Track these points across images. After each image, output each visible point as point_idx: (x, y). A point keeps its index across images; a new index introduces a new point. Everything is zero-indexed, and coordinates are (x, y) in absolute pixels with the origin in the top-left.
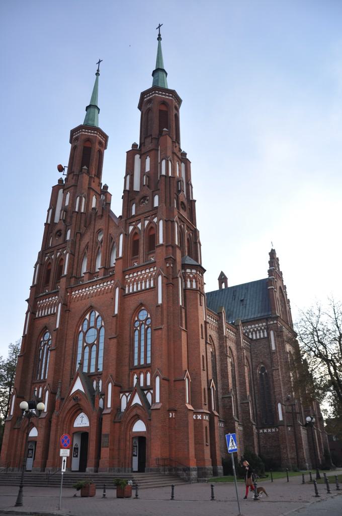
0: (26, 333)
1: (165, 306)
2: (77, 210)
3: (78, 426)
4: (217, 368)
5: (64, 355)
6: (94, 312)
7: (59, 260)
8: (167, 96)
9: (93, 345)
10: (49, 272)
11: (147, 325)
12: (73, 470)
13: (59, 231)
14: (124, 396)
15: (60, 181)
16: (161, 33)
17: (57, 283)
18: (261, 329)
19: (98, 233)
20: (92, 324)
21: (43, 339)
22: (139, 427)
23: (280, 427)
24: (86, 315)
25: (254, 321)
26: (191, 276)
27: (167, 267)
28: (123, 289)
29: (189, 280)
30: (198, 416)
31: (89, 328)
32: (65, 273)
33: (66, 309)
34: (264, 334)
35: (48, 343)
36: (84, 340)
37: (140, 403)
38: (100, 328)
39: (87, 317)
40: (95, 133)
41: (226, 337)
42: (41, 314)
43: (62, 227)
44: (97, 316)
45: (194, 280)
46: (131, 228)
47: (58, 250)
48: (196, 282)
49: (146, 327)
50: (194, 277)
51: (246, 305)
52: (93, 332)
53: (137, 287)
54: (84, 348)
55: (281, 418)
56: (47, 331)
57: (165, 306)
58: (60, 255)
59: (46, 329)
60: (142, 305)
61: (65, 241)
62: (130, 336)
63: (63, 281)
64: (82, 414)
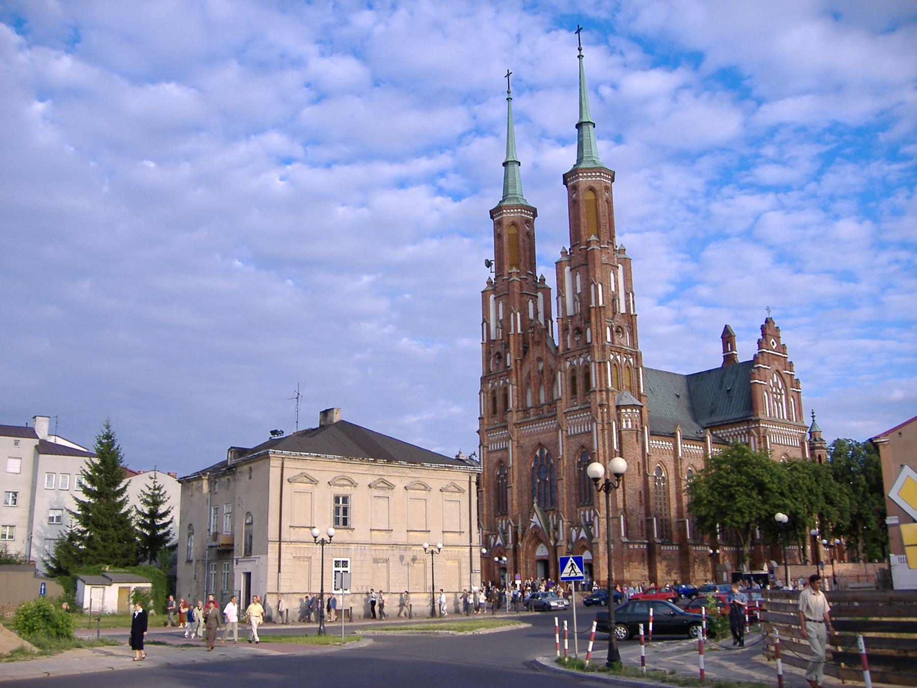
15: (489, 283)
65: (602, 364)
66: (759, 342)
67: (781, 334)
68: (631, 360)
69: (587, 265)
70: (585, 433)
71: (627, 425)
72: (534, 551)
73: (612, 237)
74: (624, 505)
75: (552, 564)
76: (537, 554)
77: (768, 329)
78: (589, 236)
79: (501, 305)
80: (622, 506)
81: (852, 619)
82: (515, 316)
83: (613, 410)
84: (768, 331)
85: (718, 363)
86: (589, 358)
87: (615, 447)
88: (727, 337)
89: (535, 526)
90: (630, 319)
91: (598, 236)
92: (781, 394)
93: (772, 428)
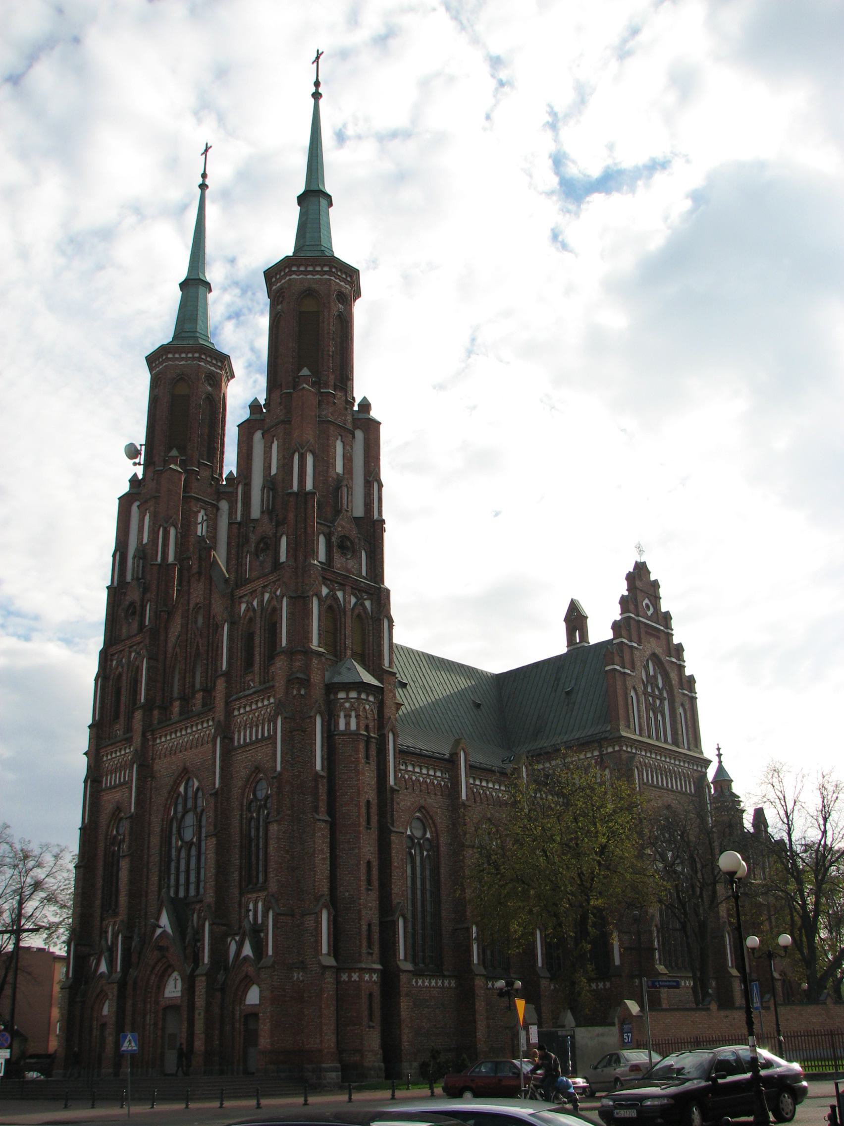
0: (86, 821)
2: (295, 488)
4: (442, 871)
5: (148, 863)
10: (118, 691)
13: (132, 604)
15: (134, 481)
16: (207, 172)
20: (190, 804)
21: (117, 831)
23: (613, 979)
24: (179, 785)
29: (342, 714)
32: (284, 644)
40: (326, 273)
42: (111, 783)
43: (267, 528)
45: (353, 714)
47: (130, 647)
48: (357, 716)
50: (352, 708)
52: (190, 819)
53: (251, 735)
54: (179, 851)
55: (617, 962)
58: (271, 599)
59: (120, 811)
61: (277, 565)
63: (138, 715)
65: (300, 603)
68: (368, 603)
71: (348, 724)
74: (333, 888)
77: (641, 586)
80: (325, 890)
81: (728, 947)
83: (318, 693)
87: (318, 767)
88: (575, 619)
89: (164, 932)
91: (315, 372)
92: (662, 700)
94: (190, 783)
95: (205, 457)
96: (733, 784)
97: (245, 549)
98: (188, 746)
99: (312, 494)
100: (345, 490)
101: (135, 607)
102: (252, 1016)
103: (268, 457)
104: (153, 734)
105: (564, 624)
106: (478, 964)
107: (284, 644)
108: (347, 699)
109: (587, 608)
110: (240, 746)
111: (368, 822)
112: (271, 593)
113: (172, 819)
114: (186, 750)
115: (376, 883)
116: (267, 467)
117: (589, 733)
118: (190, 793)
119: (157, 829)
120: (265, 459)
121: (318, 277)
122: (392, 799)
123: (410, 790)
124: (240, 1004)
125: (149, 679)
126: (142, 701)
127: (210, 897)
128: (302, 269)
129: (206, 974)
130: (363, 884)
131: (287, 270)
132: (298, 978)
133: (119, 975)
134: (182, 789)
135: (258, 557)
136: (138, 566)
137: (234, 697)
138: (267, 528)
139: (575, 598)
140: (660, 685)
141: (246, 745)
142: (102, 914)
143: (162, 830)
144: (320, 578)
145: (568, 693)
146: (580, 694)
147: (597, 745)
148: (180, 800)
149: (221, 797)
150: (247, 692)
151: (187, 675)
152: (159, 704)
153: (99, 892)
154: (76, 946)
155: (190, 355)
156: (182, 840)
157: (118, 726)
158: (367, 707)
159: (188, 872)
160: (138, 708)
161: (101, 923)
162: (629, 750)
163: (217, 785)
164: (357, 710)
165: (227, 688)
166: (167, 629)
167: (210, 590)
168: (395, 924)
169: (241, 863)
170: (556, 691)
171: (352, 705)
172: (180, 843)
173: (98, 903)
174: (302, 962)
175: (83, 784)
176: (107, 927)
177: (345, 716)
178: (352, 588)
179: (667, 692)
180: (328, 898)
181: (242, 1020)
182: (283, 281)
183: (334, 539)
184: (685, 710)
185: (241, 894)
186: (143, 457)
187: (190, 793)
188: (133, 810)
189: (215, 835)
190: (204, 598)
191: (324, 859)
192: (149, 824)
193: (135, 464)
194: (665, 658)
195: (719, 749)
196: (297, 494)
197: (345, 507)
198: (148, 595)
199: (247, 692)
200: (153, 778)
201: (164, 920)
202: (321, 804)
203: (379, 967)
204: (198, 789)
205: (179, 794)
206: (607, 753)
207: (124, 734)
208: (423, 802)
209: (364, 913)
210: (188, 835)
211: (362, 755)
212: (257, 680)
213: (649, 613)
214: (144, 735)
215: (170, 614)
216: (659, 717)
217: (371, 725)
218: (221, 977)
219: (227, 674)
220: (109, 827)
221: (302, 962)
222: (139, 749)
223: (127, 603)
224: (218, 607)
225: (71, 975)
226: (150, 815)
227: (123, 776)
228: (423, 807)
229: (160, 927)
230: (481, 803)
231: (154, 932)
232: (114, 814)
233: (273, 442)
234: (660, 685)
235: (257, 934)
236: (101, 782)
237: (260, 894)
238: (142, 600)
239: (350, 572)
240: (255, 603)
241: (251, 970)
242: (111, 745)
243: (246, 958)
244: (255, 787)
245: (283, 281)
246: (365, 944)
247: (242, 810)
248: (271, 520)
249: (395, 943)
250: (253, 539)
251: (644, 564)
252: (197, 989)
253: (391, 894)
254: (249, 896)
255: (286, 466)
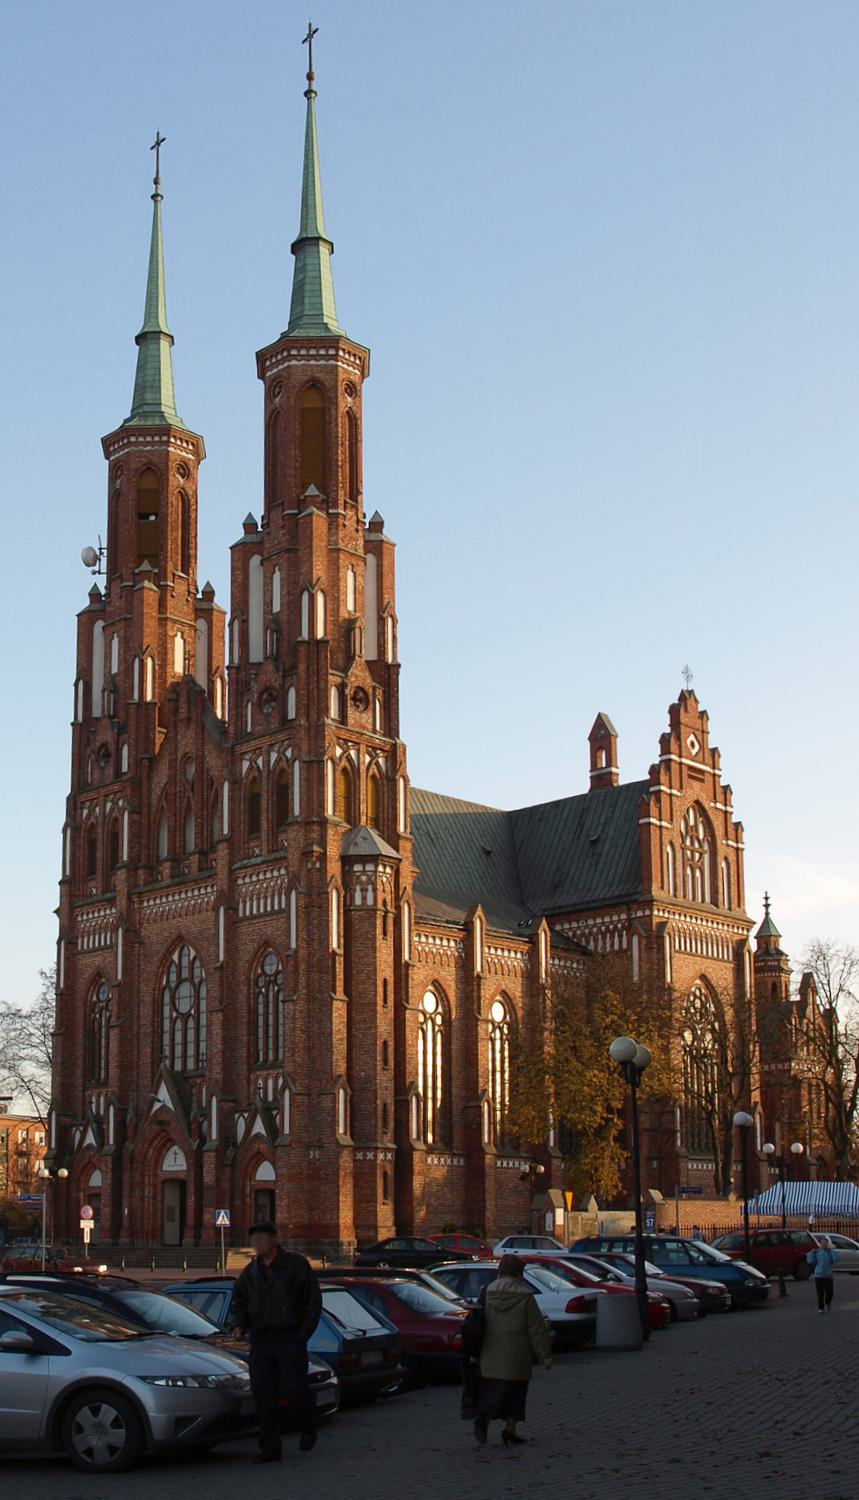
1: (302, 953)
2: (305, 635)
3: (171, 1169)
4: (453, 1047)
5: (138, 1033)
6: (186, 948)
7: (111, 820)
8: (322, 357)
9: (188, 1017)
10: (92, 844)
11: (278, 985)
12: (166, 1242)
13: (104, 745)
14: (241, 1118)
15: (94, 595)
17: (111, 875)
18: (616, 927)
19: (185, 763)
20: (185, 974)
21: (98, 997)
22: (266, 1172)
24: (172, 953)
25: (602, 907)
26: (364, 878)
27: (309, 870)
28: (232, 909)
29: (358, 888)
30: (368, 1153)
31: (180, 981)
32: (297, 812)
33: (133, 937)
34: (620, 942)
35: (107, 1006)
36: (174, 1007)
37: (264, 1132)
38: (200, 983)
39: (175, 957)
41: (479, 977)
44: (192, 956)
45: (370, 887)
46: (246, 765)
49: (276, 988)
51: (600, 855)
52: (185, 990)
53: (258, 907)
54: (173, 1022)
56: (103, 980)
57: (302, 953)
59: (101, 977)
60: (267, 944)
62: (249, 1006)
64: (175, 1148)
66: (665, 741)
67: (711, 726)
69: (295, 551)
70: (273, 912)
71: (364, 898)
72: (158, 1162)
73: (355, 493)
74: (349, 1068)
75: (191, 1189)
76: (166, 1167)
77: (684, 713)
78: (305, 487)
79: (115, 642)
82: (143, 665)
84: (684, 718)
85: (582, 786)
86: (289, 753)
87: (334, 944)
88: (602, 738)
90: (386, 674)
91: (323, 487)
93: (677, 921)
94: (185, 951)
95: (180, 568)
96: (781, 940)
97: (246, 698)
98: (183, 912)
99: (324, 642)
100: (357, 631)
101: (107, 750)
102: (268, 1192)
103: (269, 590)
104: (139, 897)
105: (588, 743)
106: (489, 1142)
107: (297, 812)
108: (364, 872)
109: (617, 724)
110: (246, 918)
111: (385, 1001)
112: (278, 752)
113: (164, 988)
114: (180, 916)
115: (391, 1063)
116: (268, 603)
117: (616, 893)
118: (185, 962)
119: (148, 999)
120: (265, 593)
121: (322, 362)
122: (407, 975)
123: (424, 963)
124: (251, 1179)
125: (132, 835)
126: (125, 859)
127: (216, 1073)
128: (303, 352)
129: (215, 1150)
130: (379, 1064)
131: (285, 354)
132: (314, 1156)
133: (113, 1148)
134: (175, 957)
135: (261, 709)
136: (109, 702)
137: (238, 865)
138: (270, 676)
139: (602, 711)
140: (701, 837)
141: (253, 917)
142: (84, 1084)
143: (153, 1000)
144: (335, 739)
145: (593, 843)
146: (607, 845)
147: (625, 907)
148: (173, 968)
149: (226, 972)
150: (253, 861)
151: (178, 833)
152: (145, 861)
153: (80, 1061)
154: (58, 1116)
155: (157, 439)
156: (177, 1011)
157: (93, 883)
158: (385, 879)
159: (185, 1044)
160: (120, 868)
161: (84, 1091)
162: (661, 914)
163: (221, 958)
164: (374, 884)
165: (230, 854)
166: (149, 779)
167: (203, 739)
168: (408, 1103)
169: (249, 1039)
170: (579, 837)
171: (369, 878)
172: (175, 1014)
173: (79, 1072)
174: (319, 1141)
175: (56, 946)
176: (90, 1096)
177: (362, 890)
178: (367, 746)
179: (709, 843)
180: (345, 1078)
181: (253, 1195)
182: (281, 367)
183: (347, 691)
184: (728, 865)
185: (250, 1071)
186: (104, 560)
187: (185, 962)
188: (120, 977)
189: (222, 1011)
190: (197, 749)
191: (342, 1039)
192: (139, 992)
193: (94, 573)
194: (708, 805)
195: (767, 898)
196: (308, 643)
197: (358, 652)
198: (125, 737)
199: (253, 861)
200: (141, 943)
201: (163, 1094)
202: (338, 984)
203: (393, 1146)
204: (195, 959)
205: (173, 962)
206: (636, 918)
207: (103, 893)
208: (436, 976)
209: (379, 1092)
210: (185, 1006)
211: (379, 930)
212: (265, 848)
213: (694, 752)
214: (129, 897)
215: (153, 761)
216: (698, 874)
217: (388, 900)
218: (230, 1153)
219: (229, 840)
220: (88, 992)
221: (319, 1141)
222: (124, 912)
223: (98, 744)
224: (213, 761)
225: (53, 1146)
226: (139, 983)
227: (105, 939)
228: (436, 981)
229: (159, 1101)
230: (496, 973)
231: (152, 1106)
232: (94, 979)
233: (274, 572)
234: (701, 837)
235: (269, 1111)
236: (77, 944)
237: (271, 1072)
238: (118, 742)
239: (364, 728)
240: (260, 762)
241: (263, 1147)
242: (89, 904)
243: (258, 1135)
244: (264, 961)
245: (281, 367)
246: (380, 1124)
247: (249, 984)
248: (277, 669)
249: (408, 1122)
250: (255, 686)
251: (691, 692)
252: (205, 1164)
253: (405, 1073)
254: (258, 1073)
255: (292, 604)
